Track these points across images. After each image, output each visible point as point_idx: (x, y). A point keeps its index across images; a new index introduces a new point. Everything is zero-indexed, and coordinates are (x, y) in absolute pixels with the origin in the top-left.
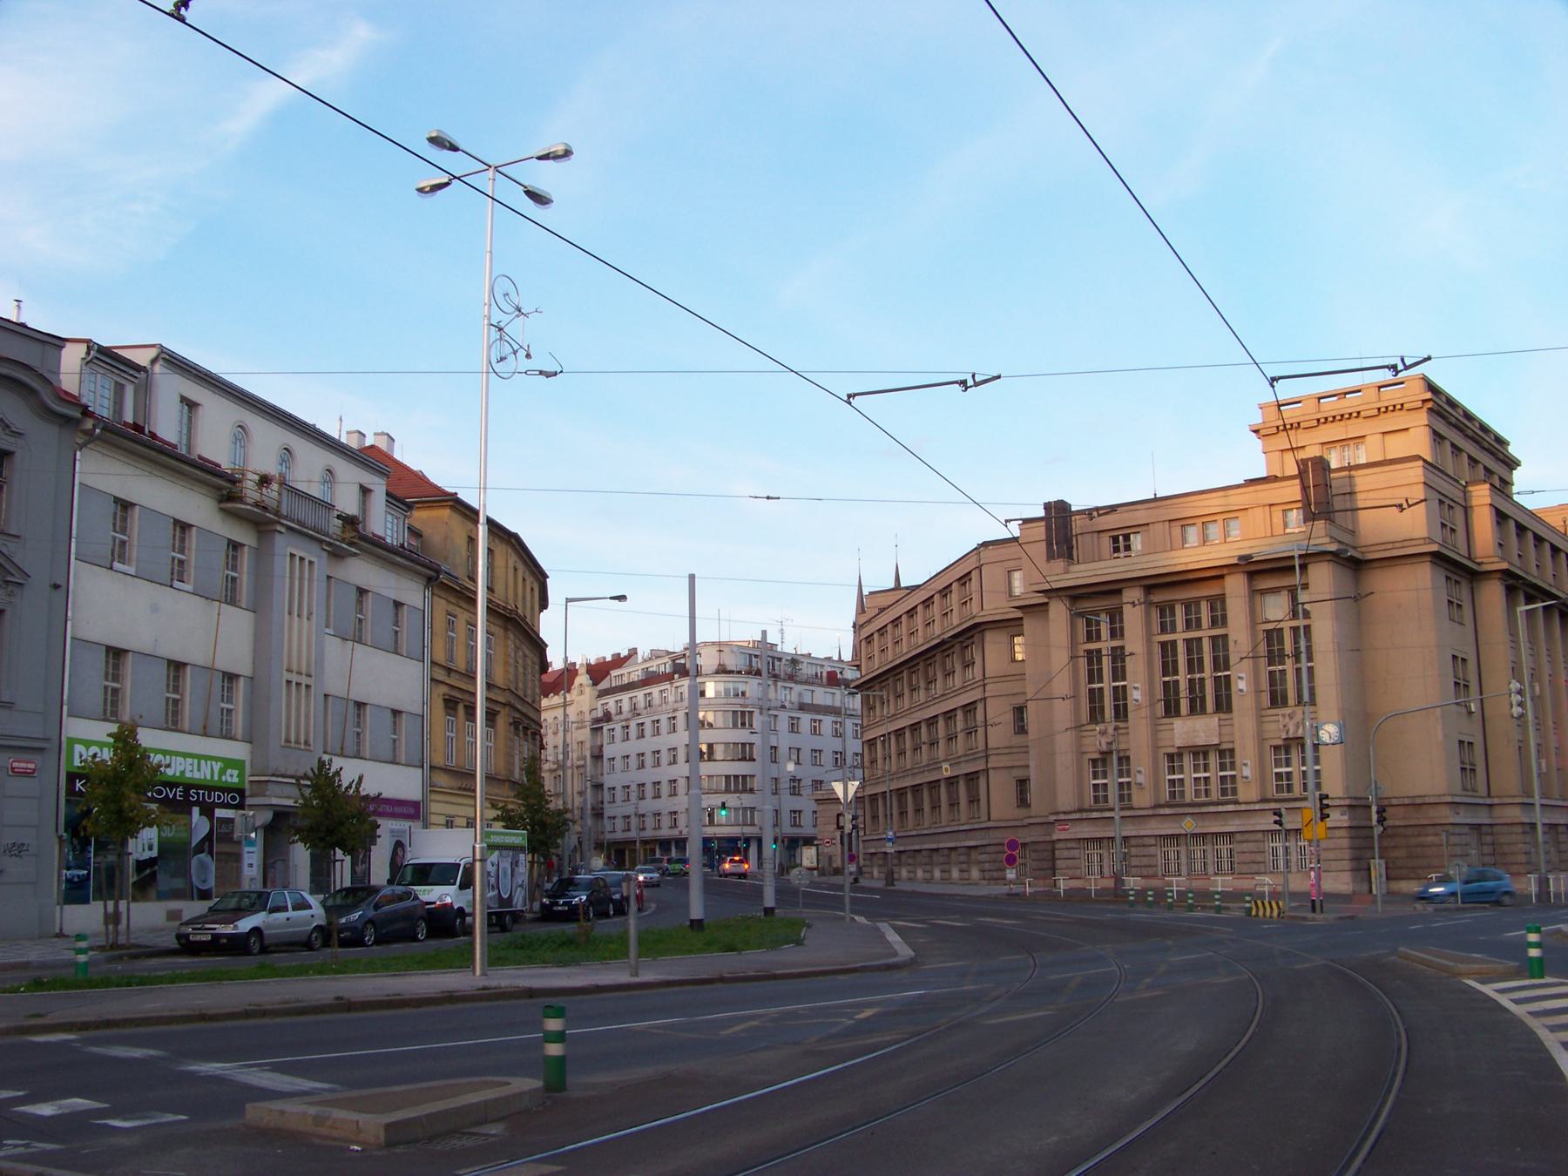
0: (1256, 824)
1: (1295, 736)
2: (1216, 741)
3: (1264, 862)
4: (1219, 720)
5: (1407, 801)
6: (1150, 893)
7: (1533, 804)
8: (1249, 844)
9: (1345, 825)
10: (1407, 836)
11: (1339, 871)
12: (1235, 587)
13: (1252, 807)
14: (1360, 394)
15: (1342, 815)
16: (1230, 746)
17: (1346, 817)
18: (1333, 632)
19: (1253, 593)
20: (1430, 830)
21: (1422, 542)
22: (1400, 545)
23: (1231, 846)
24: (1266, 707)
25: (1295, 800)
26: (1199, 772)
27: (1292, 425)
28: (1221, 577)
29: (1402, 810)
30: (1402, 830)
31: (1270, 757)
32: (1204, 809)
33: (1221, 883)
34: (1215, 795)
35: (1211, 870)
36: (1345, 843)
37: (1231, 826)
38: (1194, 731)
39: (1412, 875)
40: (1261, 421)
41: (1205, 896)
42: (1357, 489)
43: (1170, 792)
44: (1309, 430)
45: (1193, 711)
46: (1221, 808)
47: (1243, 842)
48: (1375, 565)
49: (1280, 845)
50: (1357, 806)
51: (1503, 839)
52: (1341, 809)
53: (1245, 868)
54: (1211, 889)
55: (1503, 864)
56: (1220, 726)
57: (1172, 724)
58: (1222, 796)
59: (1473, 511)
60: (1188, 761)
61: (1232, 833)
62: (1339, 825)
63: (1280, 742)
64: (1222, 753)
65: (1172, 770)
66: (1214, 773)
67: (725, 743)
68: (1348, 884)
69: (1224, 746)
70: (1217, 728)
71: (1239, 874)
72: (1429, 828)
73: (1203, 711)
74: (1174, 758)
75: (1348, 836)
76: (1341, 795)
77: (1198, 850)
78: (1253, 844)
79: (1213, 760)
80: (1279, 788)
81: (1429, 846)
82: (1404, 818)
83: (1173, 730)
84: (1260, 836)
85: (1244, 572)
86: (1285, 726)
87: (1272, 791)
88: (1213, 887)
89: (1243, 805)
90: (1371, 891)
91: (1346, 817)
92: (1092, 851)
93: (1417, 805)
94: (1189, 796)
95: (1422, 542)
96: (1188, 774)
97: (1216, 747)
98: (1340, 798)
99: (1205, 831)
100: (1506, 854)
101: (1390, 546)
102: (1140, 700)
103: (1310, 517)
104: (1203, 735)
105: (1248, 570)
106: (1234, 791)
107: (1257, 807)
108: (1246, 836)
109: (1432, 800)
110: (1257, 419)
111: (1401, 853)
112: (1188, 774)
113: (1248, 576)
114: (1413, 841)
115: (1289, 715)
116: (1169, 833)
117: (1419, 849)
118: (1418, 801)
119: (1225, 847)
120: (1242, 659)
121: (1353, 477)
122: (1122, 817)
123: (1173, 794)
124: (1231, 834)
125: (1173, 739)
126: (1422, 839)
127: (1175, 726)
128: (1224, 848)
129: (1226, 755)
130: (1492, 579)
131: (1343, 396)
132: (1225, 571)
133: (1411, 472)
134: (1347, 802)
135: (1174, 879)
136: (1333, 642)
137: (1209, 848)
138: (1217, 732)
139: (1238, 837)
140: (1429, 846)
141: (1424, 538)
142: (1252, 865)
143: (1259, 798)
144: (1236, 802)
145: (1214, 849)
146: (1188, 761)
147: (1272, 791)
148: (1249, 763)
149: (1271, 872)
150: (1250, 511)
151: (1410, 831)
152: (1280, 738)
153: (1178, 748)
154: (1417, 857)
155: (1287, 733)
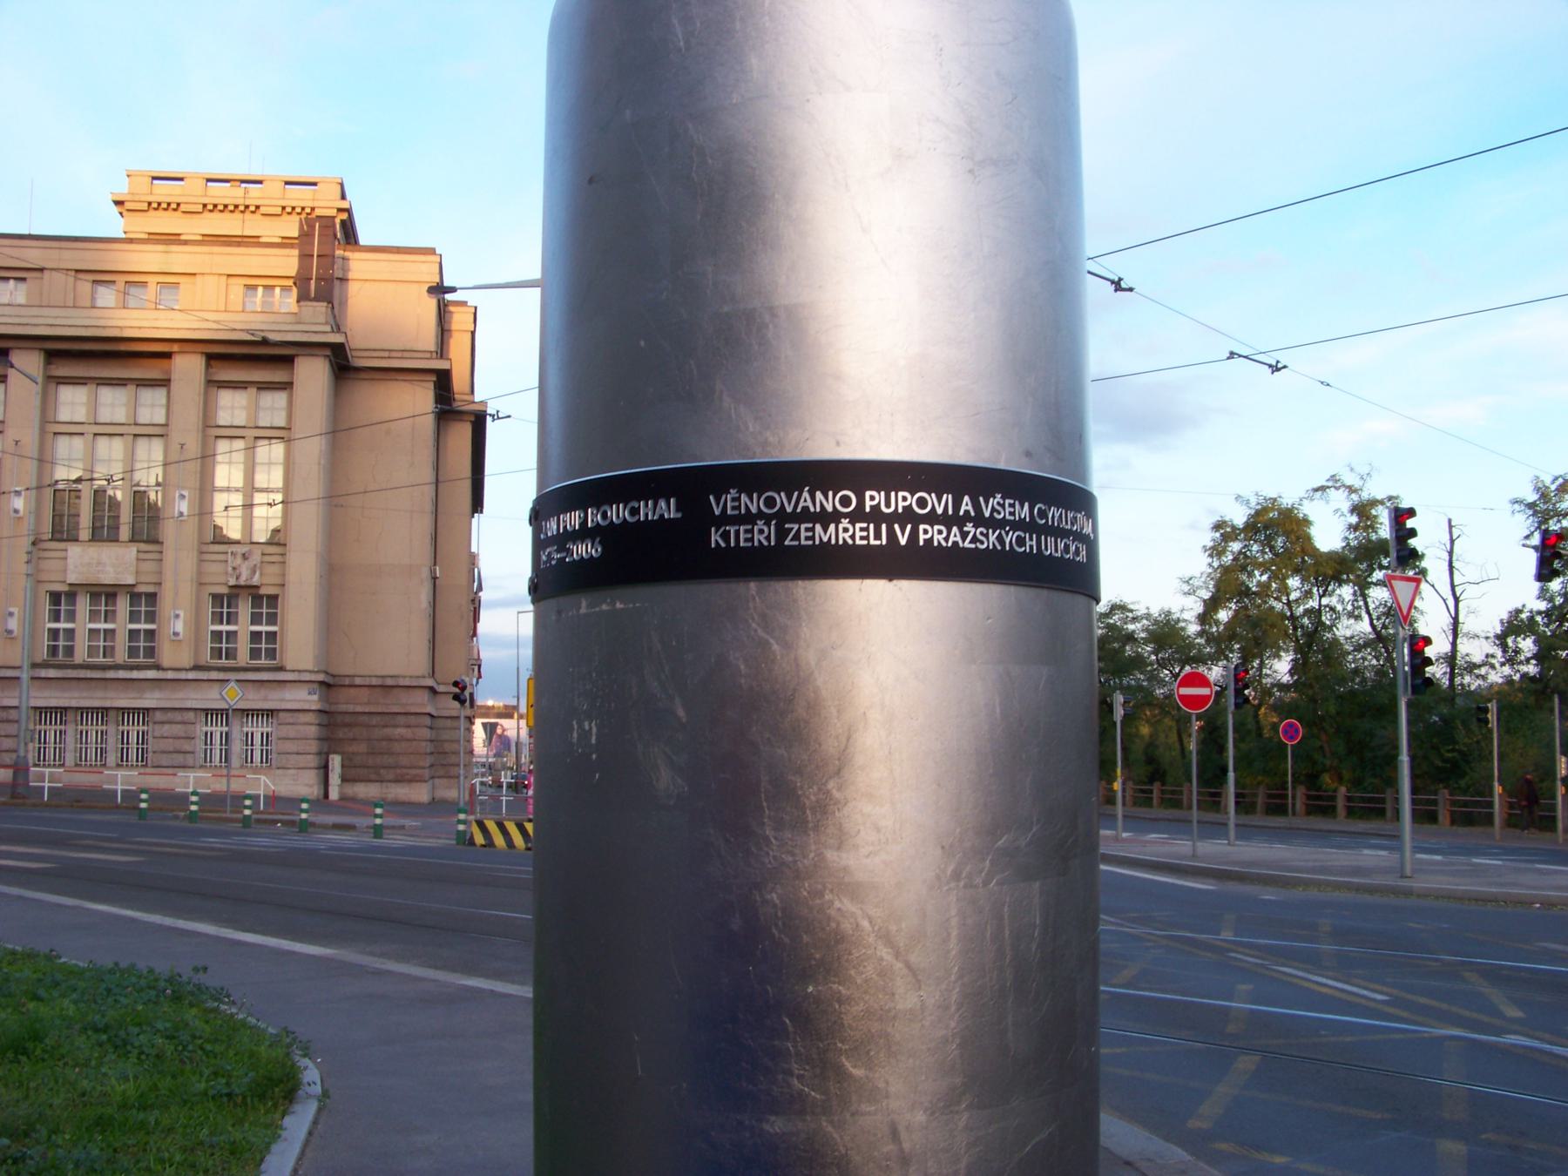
0: (188, 699)
1: (249, 583)
2: (130, 580)
3: (193, 753)
4: (138, 551)
5: (374, 682)
6: (144, 796)
7: (18, 678)
8: (174, 726)
9: (313, 708)
10: (368, 726)
11: (299, 768)
12: (188, 368)
13: (183, 675)
14: (259, 186)
15: (310, 693)
16: (151, 589)
17: (315, 697)
18: (321, 451)
19: (213, 384)
20: (402, 720)
21: (428, 355)
22: (399, 355)
23: (146, 728)
24: (209, 541)
25: (117, 667)
26: (139, 621)
27: (159, 204)
28: (167, 356)
29: (365, 691)
30: (365, 718)
31: (46, 606)
32: (111, 674)
33: (121, 780)
34: (121, 656)
35: (112, 758)
36: (313, 731)
37: (149, 700)
38: (99, 563)
39: (373, 777)
40: (126, 191)
41: (96, 800)
42: (351, 275)
43: (48, 645)
44: (188, 216)
45: (96, 537)
46: (135, 674)
47: (163, 723)
48: (362, 375)
49: (218, 730)
50: (328, 686)
51: (446, 735)
52: (306, 686)
53: (165, 760)
54: (105, 787)
55: (442, 765)
56: (138, 559)
57: (66, 550)
58: (129, 658)
59: (451, 336)
60: (83, 605)
61: (148, 709)
62: (306, 707)
63: (224, 590)
64: (135, 597)
65: (56, 617)
66: (122, 624)
67: (128, 308)
68: (311, 786)
69: (142, 589)
70: (135, 563)
71: (153, 767)
72: (399, 717)
73: (114, 539)
74: (62, 600)
75: (317, 722)
76: (310, 667)
77: (93, 730)
78: (179, 726)
79: (123, 605)
80: (217, 653)
81: (396, 740)
82: (368, 703)
83: (66, 558)
84: (191, 715)
85: (202, 353)
86: (234, 569)
87: (206, 658)
88: (109, 783)
89: (170, 672)
90: (326, 796)
91: (315, 697)
92: (48, 727)
93: (386, 688)
94: (81, 655)
95: (428, 355)
96: (83, 622)
97: (129, 589)
98: (310, 672)
99: (108, 704)
100: (446, 753)
101: (386, 354)
102: (21, 514)
103: (303, 297)
104: (111, 570)
105: (207, 351)
106: (150, 652)
107: (191, 675)
108: (170, 715)
109: (407, 682)
110: (122, 188)
111: (362, 748)
112: (83, 622)
113: (204, 359)
114: (378, 733)
115: (244, 555)
116: (52, 705)
117: (384, 743)
118: (389, 682)
119: (95, 727)
120: (1232, 355)
121: (348, 259)
122: (32, 678)
123: (53, 650)
124: (146, 711)
125: (65, 571)
126: (388, 731)
127: (70, 553)
128: (134, 731)
129: (146, 601)
130: (461, 420)
131: (238, 183)
132: (175, 348)
133: (424, 267)
134: (321, 677)
135: (47, 770)
136: (319, 464)
137: (111, 729)
138: (133, 569)
139: (159, 716)
140: (396, 740)
141: (431, 352)
142: (175, 755)
143: (192, 665)
144: (158, 667)
145: (77, 730)
146: (83, 605)
147: (206, 658)
148: (16, 613)
149: (201, 767)
150: (198, 278)
151: (375, 720)
152: (226, 584)
153: (70, 584)
154: (381, 753)
155: (237, 578)
